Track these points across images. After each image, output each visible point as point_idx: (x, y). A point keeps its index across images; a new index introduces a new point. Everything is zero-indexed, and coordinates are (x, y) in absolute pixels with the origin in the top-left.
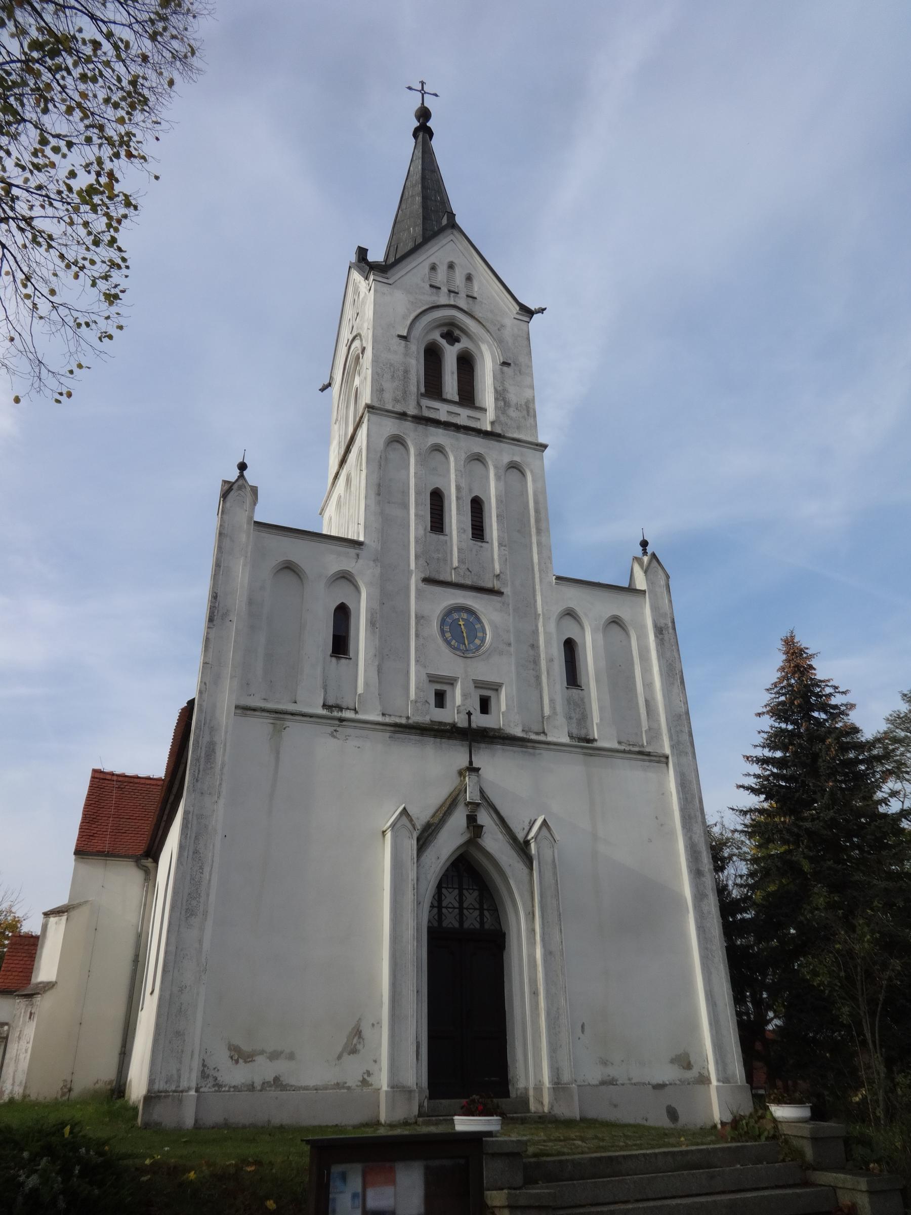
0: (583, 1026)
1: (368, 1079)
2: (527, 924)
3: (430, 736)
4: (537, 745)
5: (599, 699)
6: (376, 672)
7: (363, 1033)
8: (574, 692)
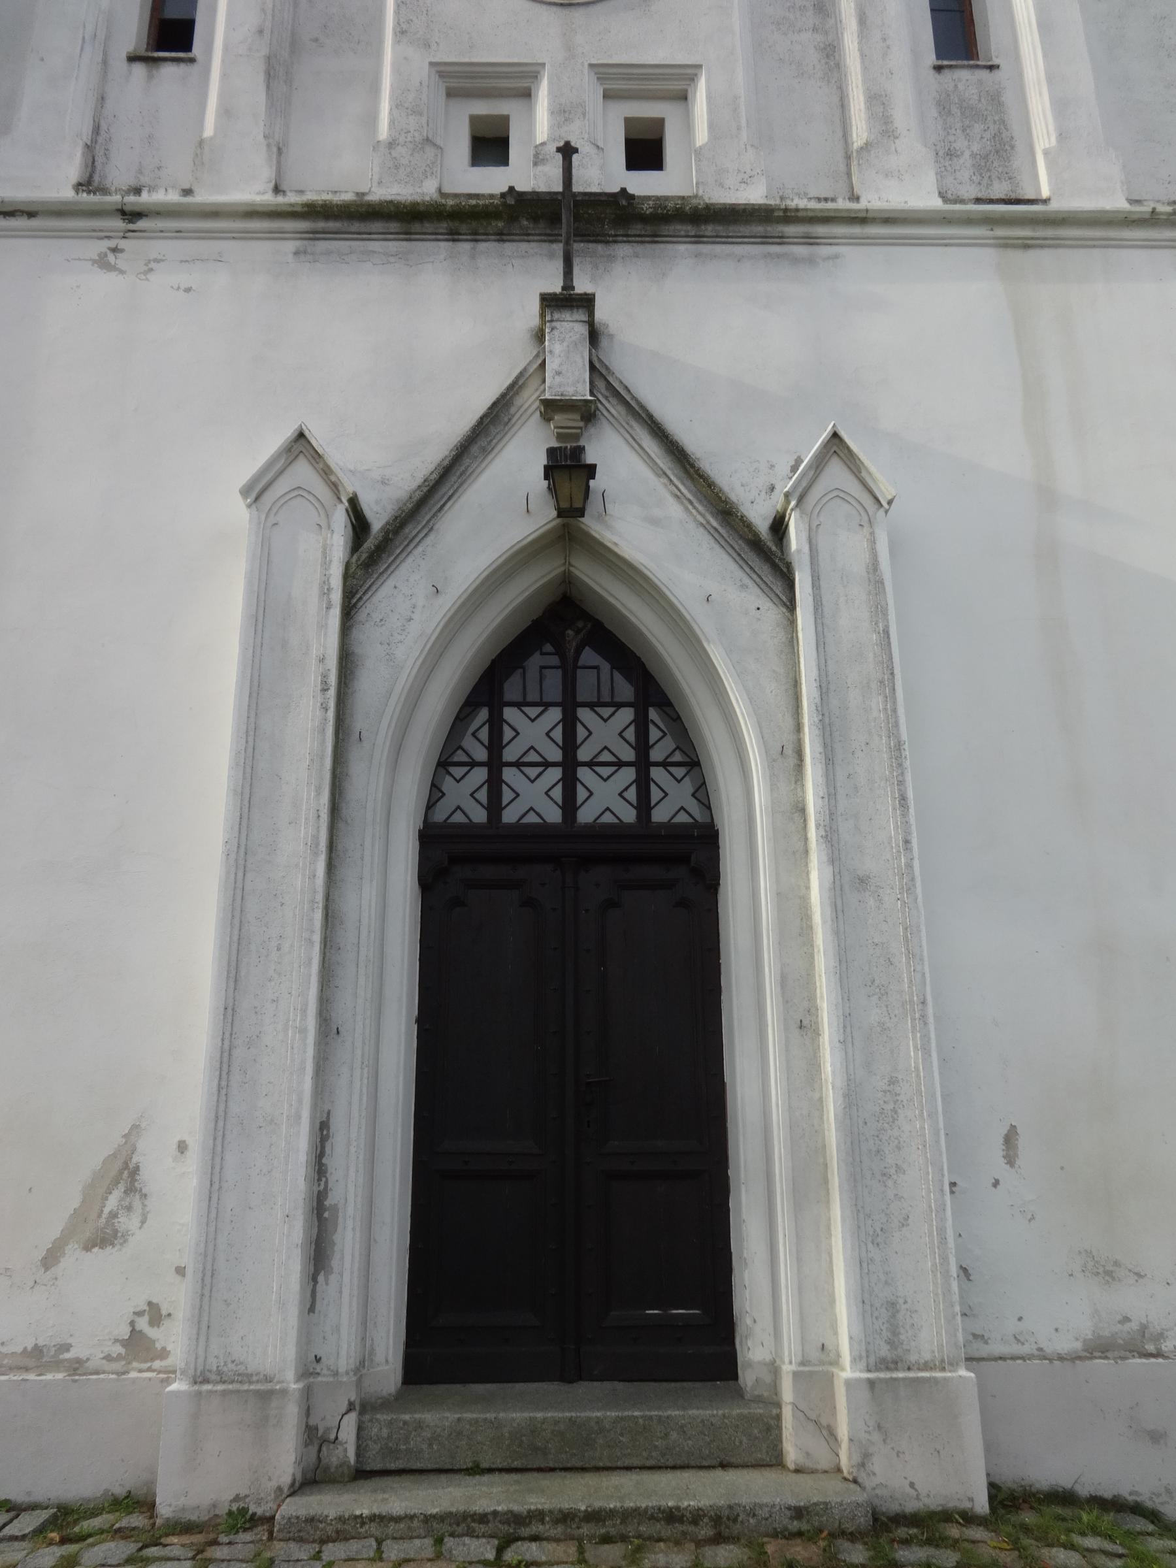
0: (1010, 1139)
1: (151, 1332)
2: (773, 787)
3: (435, 236)
4: (820, 230)
5: (1051, 79)
6: (261, 78)
7: (144, 1175)
8: (964, 79)
